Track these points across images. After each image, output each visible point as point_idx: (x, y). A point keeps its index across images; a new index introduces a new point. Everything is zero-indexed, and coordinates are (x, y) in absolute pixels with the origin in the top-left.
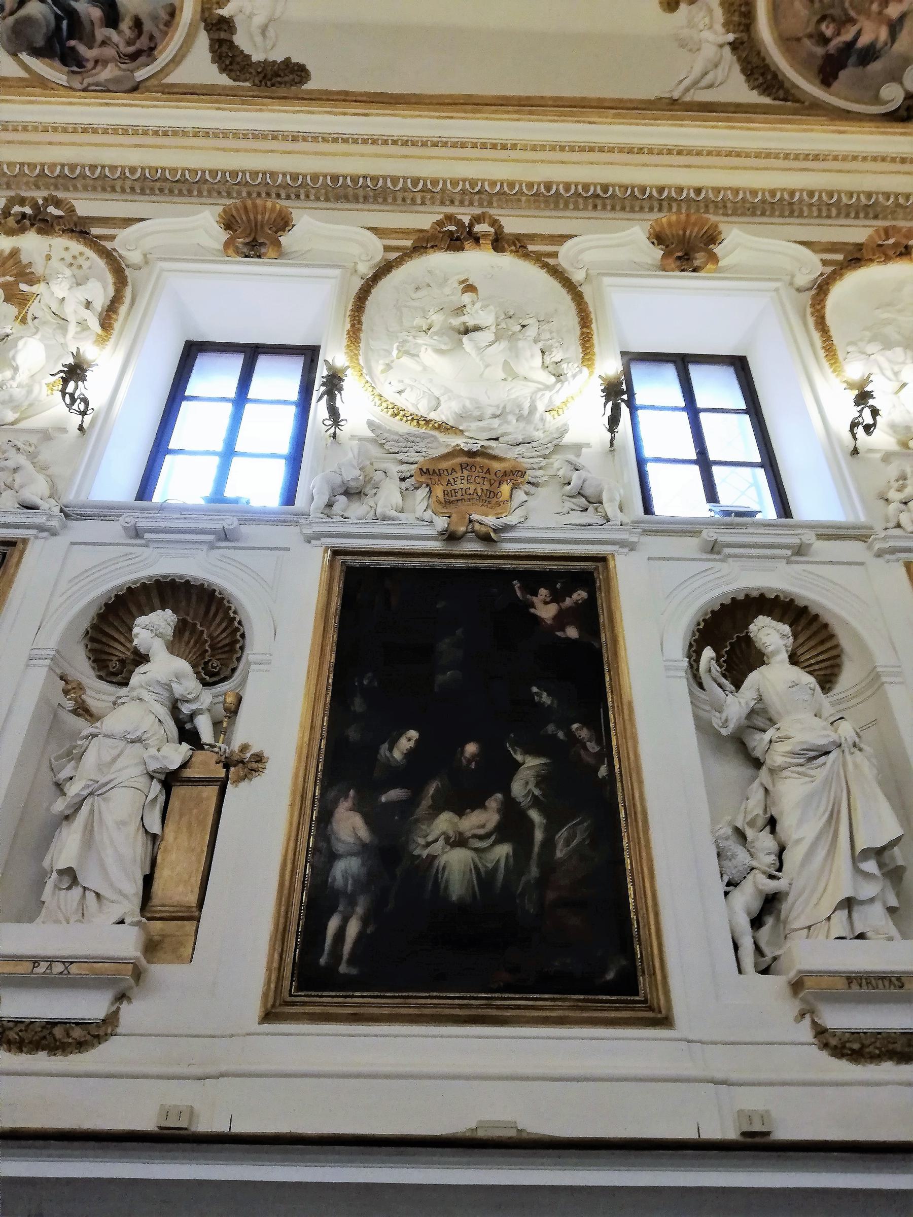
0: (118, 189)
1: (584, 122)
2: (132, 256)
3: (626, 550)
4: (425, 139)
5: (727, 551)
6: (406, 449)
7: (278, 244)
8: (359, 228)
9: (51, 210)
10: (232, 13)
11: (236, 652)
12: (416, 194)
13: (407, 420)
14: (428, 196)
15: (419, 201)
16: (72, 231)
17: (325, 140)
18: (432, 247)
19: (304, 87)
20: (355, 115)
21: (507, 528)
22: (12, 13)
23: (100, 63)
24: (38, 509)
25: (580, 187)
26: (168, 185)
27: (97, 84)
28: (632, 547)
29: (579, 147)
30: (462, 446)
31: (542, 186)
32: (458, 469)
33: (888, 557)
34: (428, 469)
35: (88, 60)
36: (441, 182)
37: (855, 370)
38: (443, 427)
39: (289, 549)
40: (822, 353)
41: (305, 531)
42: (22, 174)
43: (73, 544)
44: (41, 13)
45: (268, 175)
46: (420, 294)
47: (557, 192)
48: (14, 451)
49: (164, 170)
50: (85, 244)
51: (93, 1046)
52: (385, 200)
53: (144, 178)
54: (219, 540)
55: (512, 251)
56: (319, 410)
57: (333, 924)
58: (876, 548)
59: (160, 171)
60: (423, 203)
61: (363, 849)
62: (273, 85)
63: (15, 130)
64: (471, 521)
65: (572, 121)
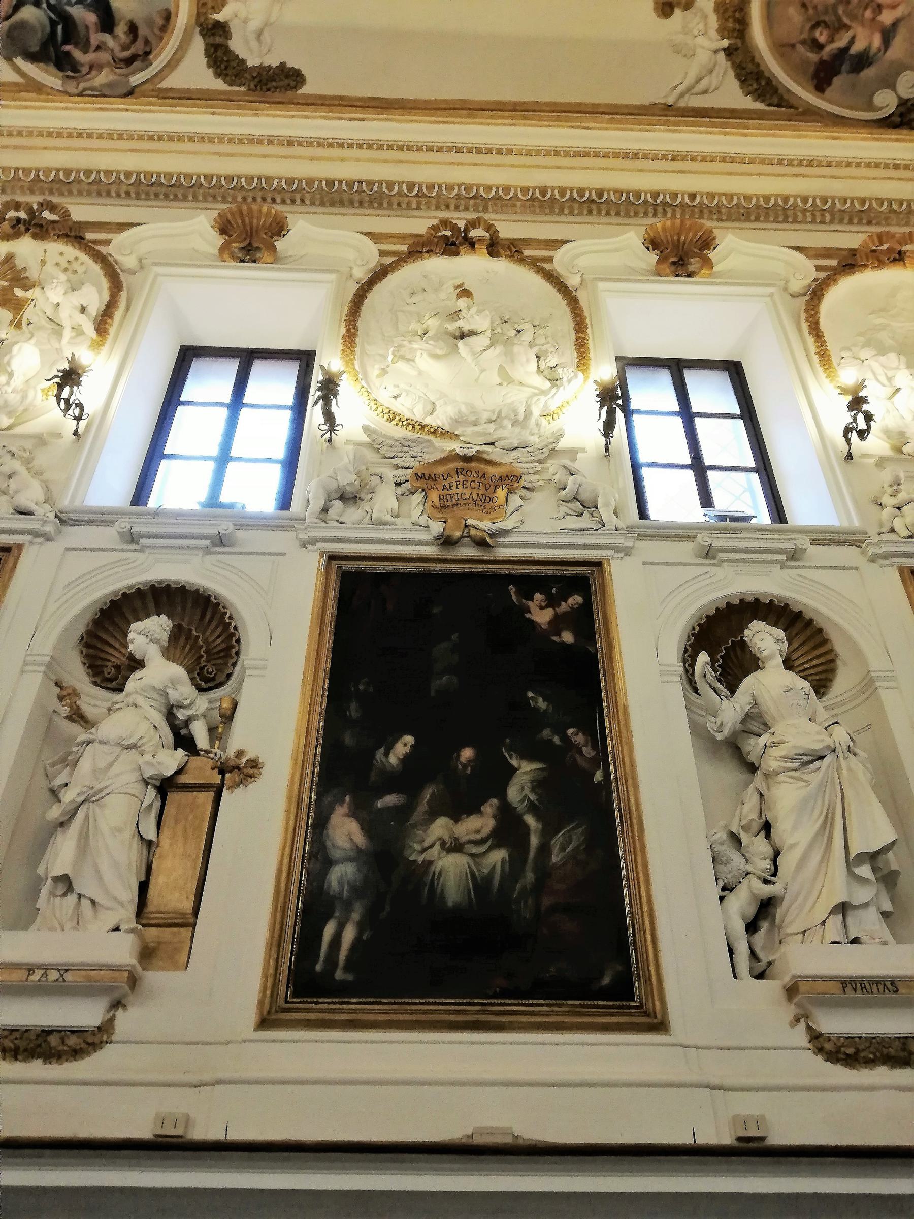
3: (621, 555)
4: (420, 144)
5: (721, 555)
6: (402, 454)
9: (47, 215)
10: (227, 18)
12: (411, 199)
13: (403, 425)
14: (424, 200)
15: (414, 206)
16: (67, 236)
17: (320, 145)
18: (428, 252)
19: (300, 92)
21: (504, 533)
28: (627, 552)
30: (458, 450)
32: (454, 473)
34: (423, 474)
35: (82, 65)
36: (436, 187)
37: (848, 375)
38: (438, 432)
39: (283, 554)
40: (816, 358)
43: (67, 549)
46: (415, 299)
48: (9, 456)
49: (159, 174)
50: (80, 249)
51: (89, 1054)
52: (381, 204)
53: (138, 183)
54: (215, 545)
55: (507, 256)
56: (315, 415)
57: (329, 930)
60: (418, 208)
61: (358, 855)
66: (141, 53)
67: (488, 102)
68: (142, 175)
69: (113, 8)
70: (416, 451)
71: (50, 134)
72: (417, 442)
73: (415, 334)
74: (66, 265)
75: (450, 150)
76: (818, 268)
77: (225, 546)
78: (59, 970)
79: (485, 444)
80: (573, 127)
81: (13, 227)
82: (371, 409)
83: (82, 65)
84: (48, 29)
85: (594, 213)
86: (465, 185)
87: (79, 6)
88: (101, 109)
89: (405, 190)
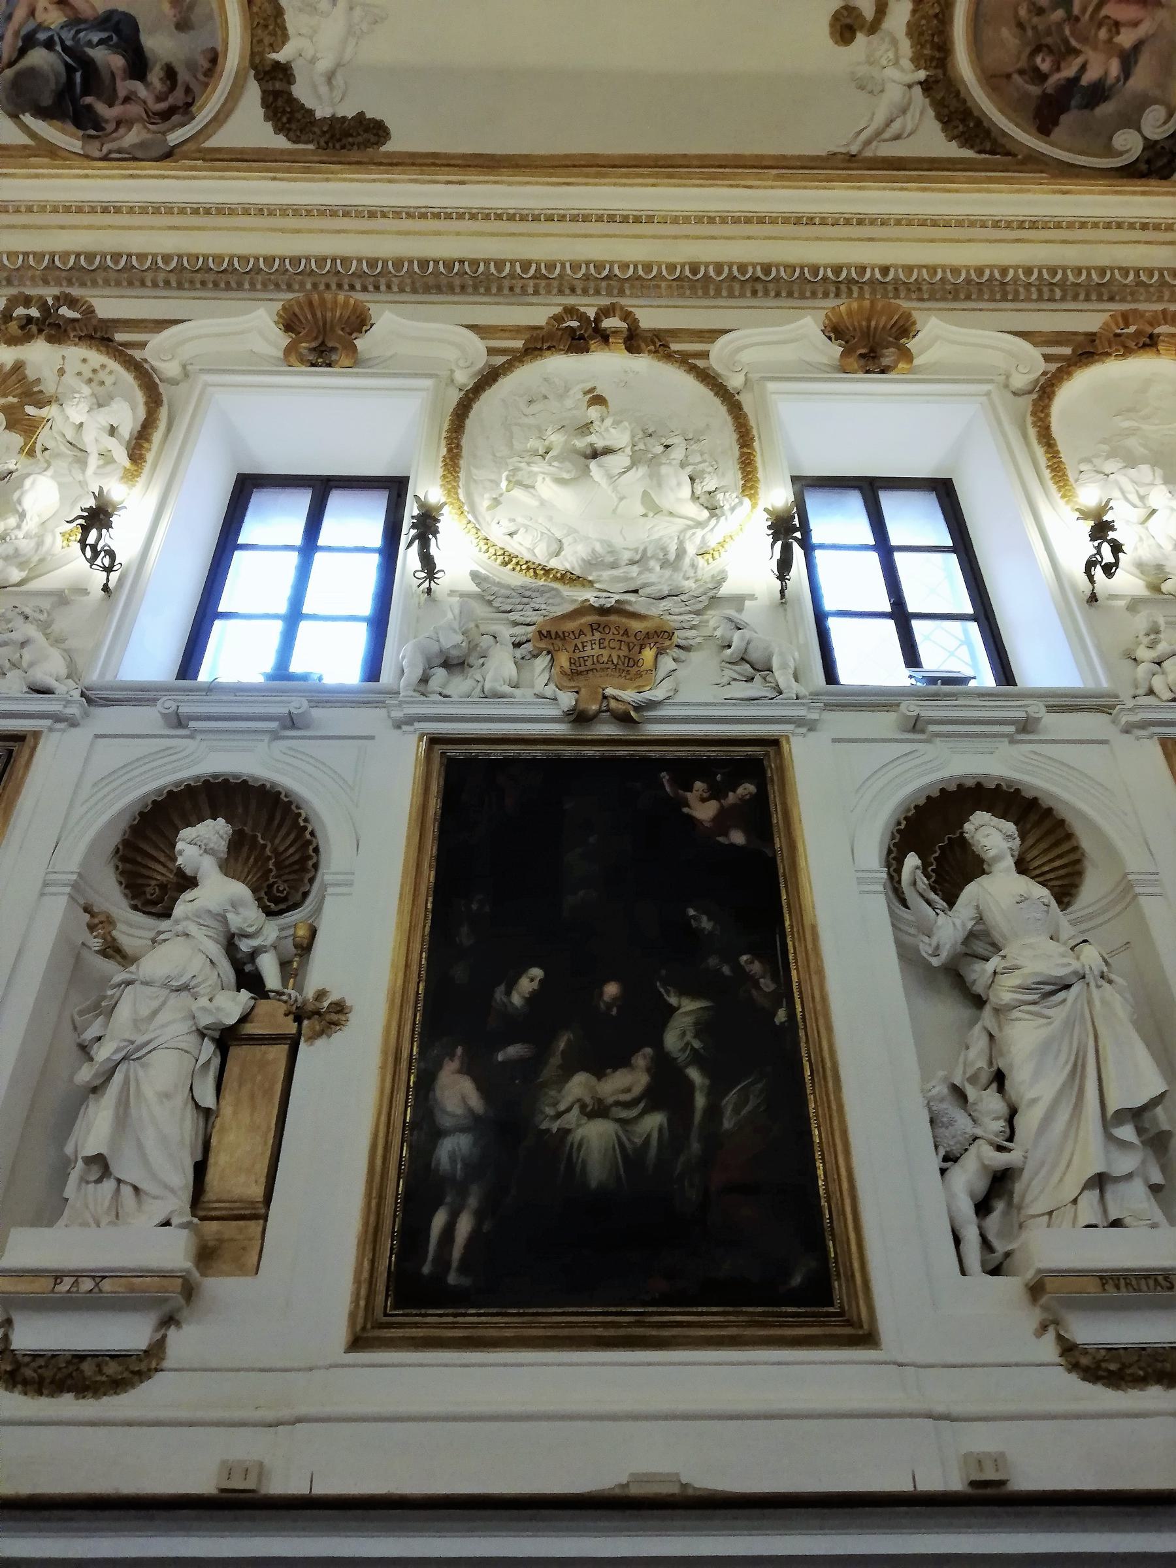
1: (737, 186)
2: (169, 368)
3: (804, 730)
4: (537, 212)
5: (932, 728)
9: (64, 311)
13: (521, 570)
14: (543, 283)
15: (531, 290)
16: (91, 337)
17: (410, 216)
18: (549, 348)
19: (383, 149)
21: (652, 705)
22: (11, 64)
25: (735, 268)
26: (210, 277)
30: (592, 600)
32: (587, 630)
35: (107, 121)
36: (558, 266)
37: (1089, 495)
38: (568, 578)
39: (372, 738)
40: (1047, 474)
41: (394, 714)
42: (26, 266)
43: (97, 736)
45: (339, 262)
46: (535, 408)
48: (21, 619)
49: (206, 258)
51: (133, 1386)
53: (180, 268)
55: (650, 352)
56: (409, 558)
57: (439, 1220)
58: (1124, 720)
59: (201, 260)
60: (536, 293)
62: (343, 147)
64: (605, 697)
66: (180, 104)
68: (185, 259)
69: (148, 54)
71: (67, 209)
72: (541, 591)
73: (535, 453)
75: (574, 219)
76: (1047, 358)
77: (299, 729)
78: (93, 1277)
82: (480, 551)
84: (63, 79)
85: (760, 294)
88: (132, 176)
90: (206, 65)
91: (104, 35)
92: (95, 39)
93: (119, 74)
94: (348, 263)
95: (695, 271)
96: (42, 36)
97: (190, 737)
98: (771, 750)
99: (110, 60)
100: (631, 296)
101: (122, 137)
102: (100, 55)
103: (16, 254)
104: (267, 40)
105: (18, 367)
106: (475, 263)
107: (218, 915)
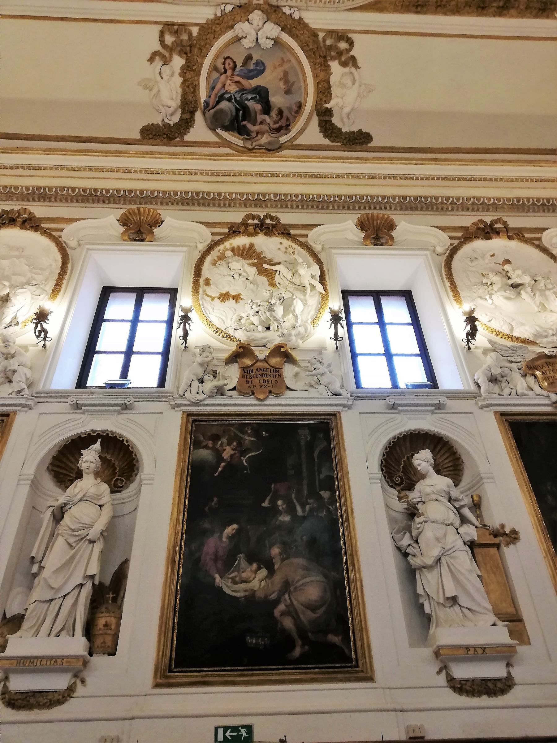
0: (289, 206)
1: (537, 166)
2: (73, 243)
3: (346, 409)
4: (454, 177)
5: (399, 408)
7: (392, 238)
8: (429, 227)
10: (332, 107)
11: (388, 478)
12: (448, 205)
13: (505, 338)
14: (455, 206)
17: (401, 178)
18: (475, 237)
19: (370, 145)
20: (416, 164)
22: (213, 108)
23: (259, 134)
24: (341, 395)
25: (535, 200)
26: (315, 204)
27: (260, 145)
28: (349, 407)
29: (536, 179)
30: (547, 353)
31: (515, 200)
32: (545, 365)
33: (485, 409)
34: (530, 366)
35: (253, 132)
36: (461, 199)
38: (527, 341)
43: (41, 414)
44: (229, 108)
46: (474, 264)
47: (523, 202)
48: (319, 363)
49: (313, 195)
52: (432, 209)
53: (302, 200)
54: (123, 409)
55: (517, 239)
59: (311, 196)
60: (452, 210)
62: (353, 144)
63: (234, 175)
65: (531, 166)
66: (284, 125)
67: (471, 148)
68: (304, 196)
69: (271, 104)
70: (519, 352)
72: (520, 348)
74: (285, 250)
75: (470, 179)
79: (554, 347)
80: (534, 166)
81: (255, 229)
82: (484, 329)
83: (253, 132)
84: (234, 114)
85: (546, 211)
86: (477, 197)
87: (252, 101)
89: (445, 201)
90: (296, 109)
91: (254, 96)
92: (249, 97)
93: (258, 112)
94: (362, 198)
95: (518, 201)
96: (227, 96)
97: (83, 413)
98: (333, 419)
99: (255, 106)
100: (492, 211)
101: (260, 139)
102: (251, 104)
103: (232, 193)
104: (324, 99)
105: (252, 246)
106: (426, 198)
107: (448, 492)
